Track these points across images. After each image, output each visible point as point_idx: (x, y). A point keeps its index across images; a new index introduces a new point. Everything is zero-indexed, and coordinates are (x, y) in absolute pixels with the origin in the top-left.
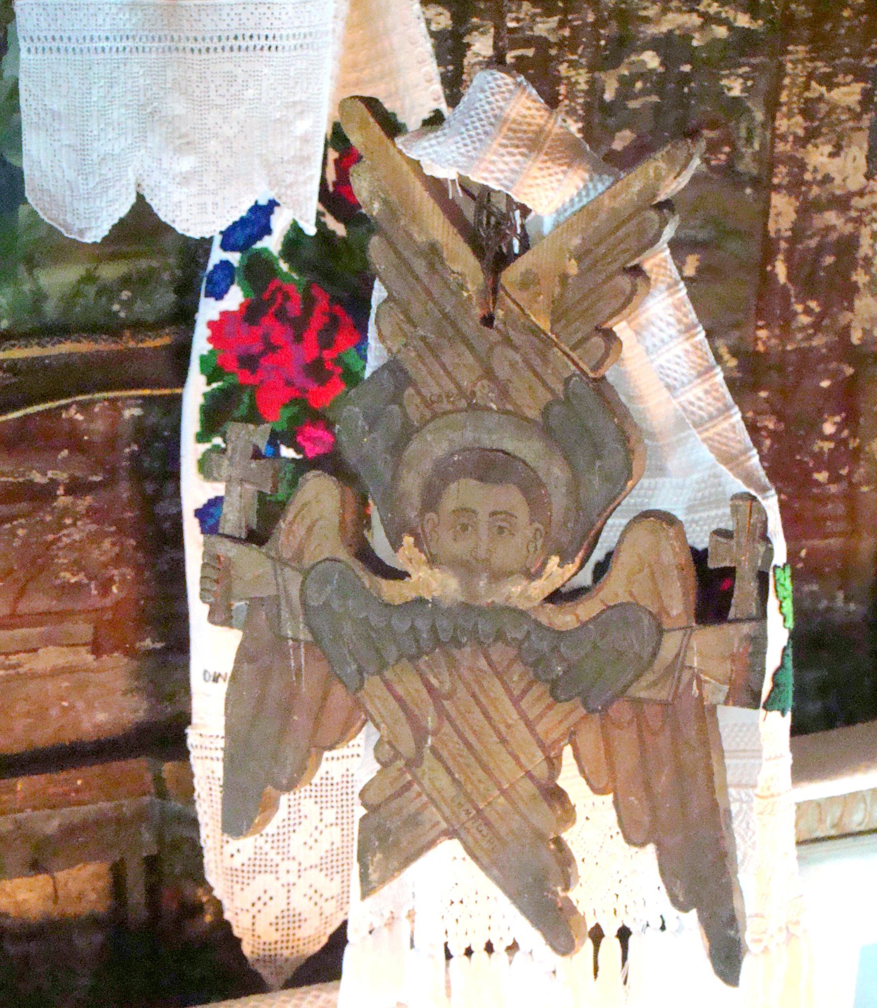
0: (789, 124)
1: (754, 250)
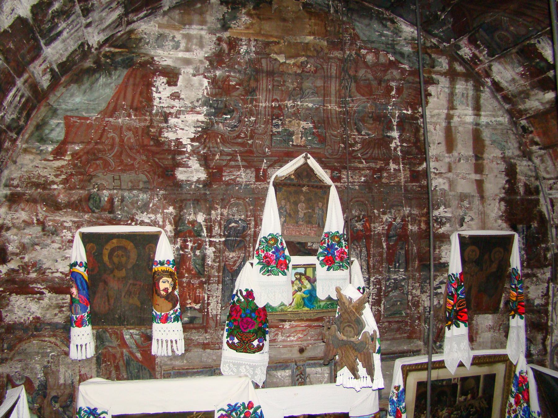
0: (410, 288)
1: (406, 301)
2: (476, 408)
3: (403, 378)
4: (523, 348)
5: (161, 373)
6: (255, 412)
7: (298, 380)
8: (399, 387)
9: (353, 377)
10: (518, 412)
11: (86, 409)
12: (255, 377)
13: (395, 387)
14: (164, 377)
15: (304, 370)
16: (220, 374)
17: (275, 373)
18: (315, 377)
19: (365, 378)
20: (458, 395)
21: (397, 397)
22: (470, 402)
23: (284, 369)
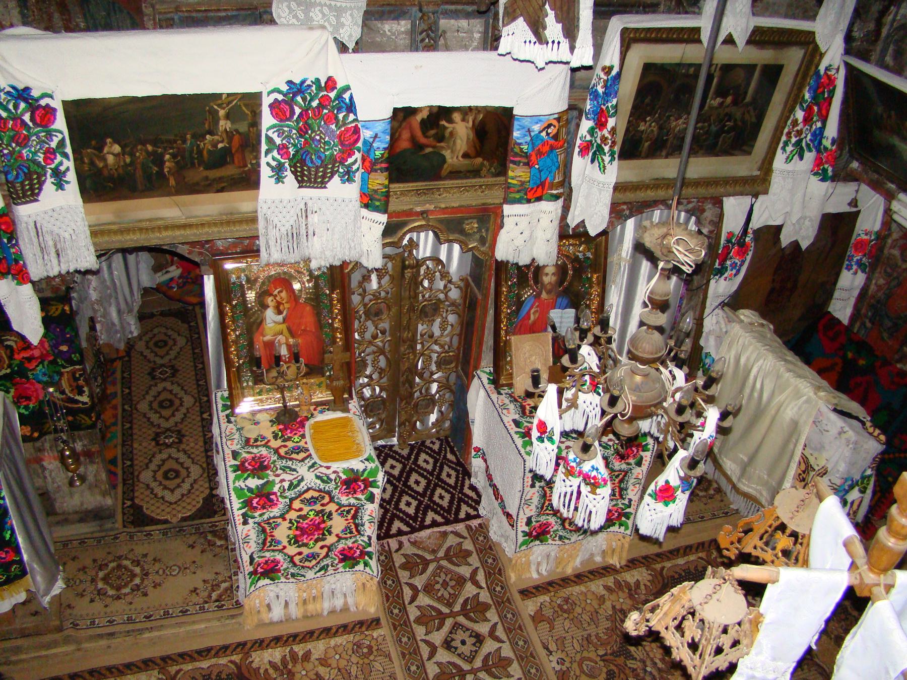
2: (736, 120)
3: (621, 53)
4: (844, 25)
5: (154, 19)
6: (339, 97)
7: (422, 40)
8: (611, 68)
9: (534, 39)
10: (803, 136)
11: (8, 89)
12: (341, 31)
13: (604, 69)
14: (161, 27)
15: (436, 23)
16: (272, 22)
17: (379, 25)
18: (454, 37)
19: (556, 45)
20: (710, 96)
21: (605, 86)
22: (727, 110)
23: (396, 18)
